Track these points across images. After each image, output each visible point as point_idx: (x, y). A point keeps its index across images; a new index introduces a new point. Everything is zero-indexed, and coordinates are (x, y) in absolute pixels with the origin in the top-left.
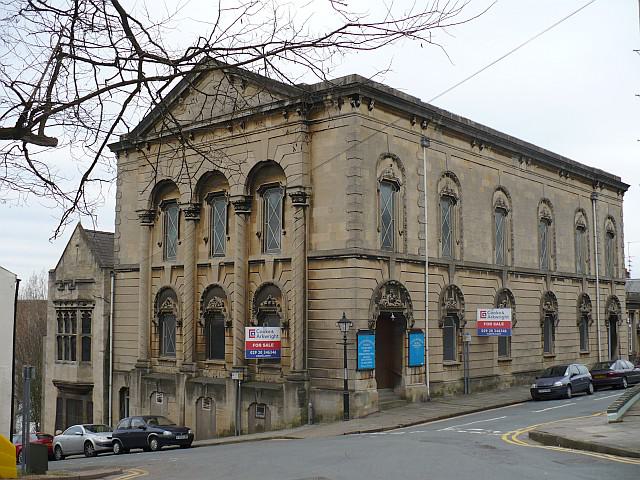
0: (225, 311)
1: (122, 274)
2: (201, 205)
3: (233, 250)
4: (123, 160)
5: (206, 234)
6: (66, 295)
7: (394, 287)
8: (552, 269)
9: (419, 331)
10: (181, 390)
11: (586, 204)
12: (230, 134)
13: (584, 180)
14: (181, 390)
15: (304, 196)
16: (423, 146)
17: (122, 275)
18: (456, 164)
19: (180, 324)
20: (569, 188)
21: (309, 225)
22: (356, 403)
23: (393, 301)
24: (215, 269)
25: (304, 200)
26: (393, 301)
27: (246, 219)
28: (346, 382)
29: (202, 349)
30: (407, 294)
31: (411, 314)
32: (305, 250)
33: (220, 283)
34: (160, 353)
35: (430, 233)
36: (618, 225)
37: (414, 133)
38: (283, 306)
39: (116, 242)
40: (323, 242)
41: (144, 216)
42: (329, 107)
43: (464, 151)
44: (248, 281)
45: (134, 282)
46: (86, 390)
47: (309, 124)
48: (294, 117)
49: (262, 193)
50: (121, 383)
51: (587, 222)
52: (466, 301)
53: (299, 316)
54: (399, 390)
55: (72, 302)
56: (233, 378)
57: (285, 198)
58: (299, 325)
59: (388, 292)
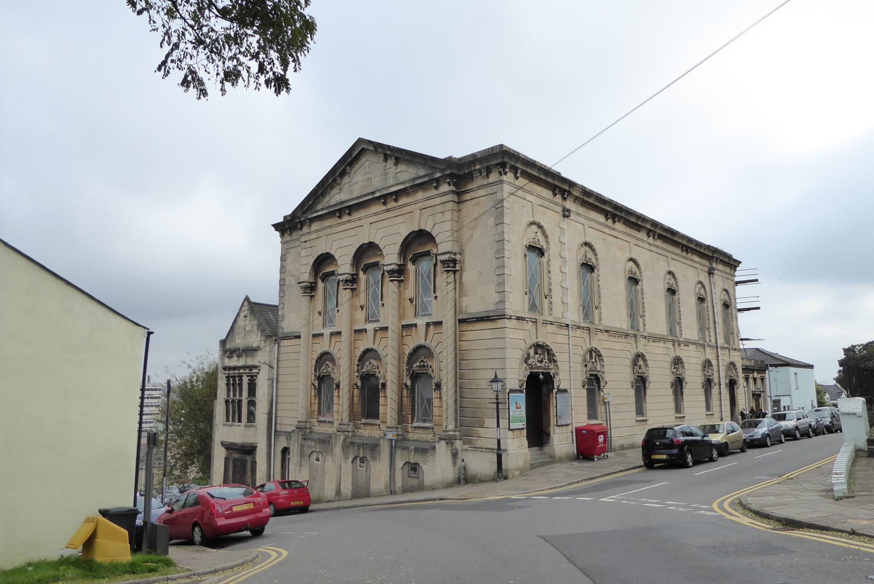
0: (379, 373)
1: (285, 341)
2: (357, 275)
3: (388, 316)
4: (287, 237)
5: (362, 302)
6: (234, 362)
7: (540, 348)
8: (679, 336)
9: (565, 391)
10: (338, 450)
11: (704, 278)
12: (384, 208)
13: (702, 255)
14: (338, 450)
15: (454, 261)
16: (564, 216)
17: (285, 343)
18: (593, 237)
19: (338, 386)
20: (689, 263)
21: (459, 288)
22: (509, 462)
23: (541, 362)
24: (370, 333)
25: (452, 265)
26: (541, 362)
27: (400, 286)
28: (499, 441)
29: (358, 409)
30: (553, 355)
31: (557, 374)
32: (455, 313)
33: (375, 347)
34: (319, 413)
35: (573, 300)
36: (732, 298)
37: (555, 204)
38: (434, 367)
39: (280, 313)
40: (474, 305)
41: (306, 288)
42: (477, 177)
43: (600, 223)
44: (401, 344)
45: (296, 349)
46: (250, 450)
47: (459, 194)
48: (445, 188)
49: (414, 260)
50: (282, 443)
51: (706, 293)
52: (605, 363)
53: (451, 375)
54: (546, 449)
55: (239, 368)
56: (387, 437)
57: (435, 265)
58: (451, 384)
59: (536, 353)
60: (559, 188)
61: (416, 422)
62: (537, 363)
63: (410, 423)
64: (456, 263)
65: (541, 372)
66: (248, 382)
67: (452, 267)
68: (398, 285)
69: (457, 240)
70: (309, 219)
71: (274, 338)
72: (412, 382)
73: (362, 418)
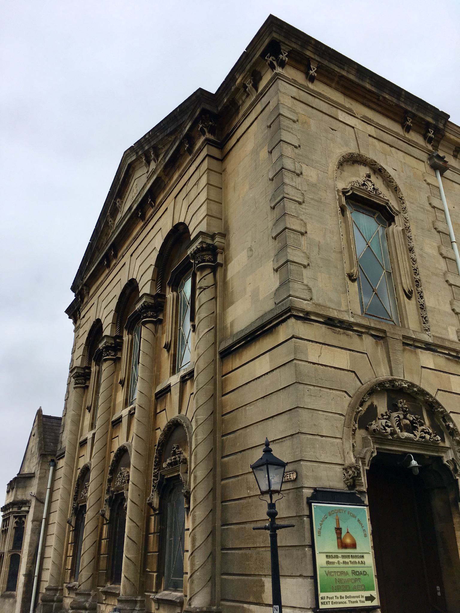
23: (411, 428)
26: (411, 428)
30: (446, 417)
60: (414, 116)
61: (164, 590)
62: (398, 430)
63: (154, 590)
64: (218, 254)
65: (413, 454)
66: (15, 526)
67: (208, 261)
68: (153, 330)
69: (219, 216)
70: (85, 285)
71: (49, 458)
72: (161, 499)
73: (106, 581)
